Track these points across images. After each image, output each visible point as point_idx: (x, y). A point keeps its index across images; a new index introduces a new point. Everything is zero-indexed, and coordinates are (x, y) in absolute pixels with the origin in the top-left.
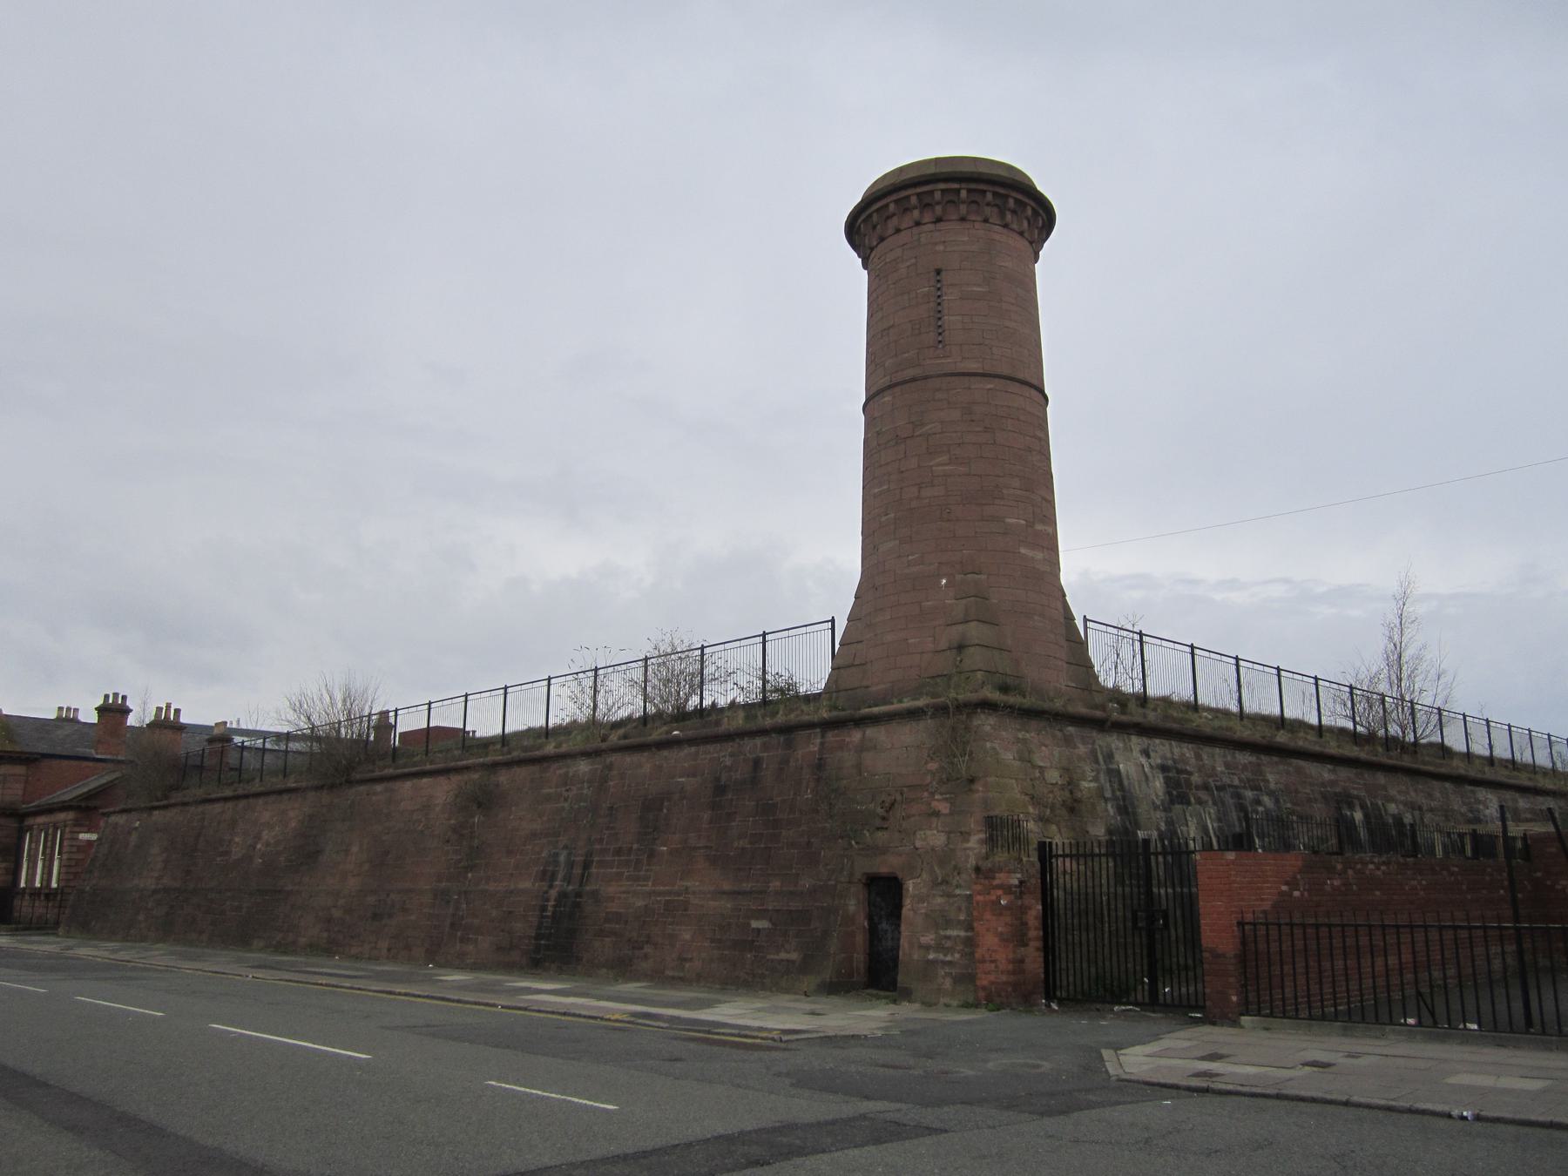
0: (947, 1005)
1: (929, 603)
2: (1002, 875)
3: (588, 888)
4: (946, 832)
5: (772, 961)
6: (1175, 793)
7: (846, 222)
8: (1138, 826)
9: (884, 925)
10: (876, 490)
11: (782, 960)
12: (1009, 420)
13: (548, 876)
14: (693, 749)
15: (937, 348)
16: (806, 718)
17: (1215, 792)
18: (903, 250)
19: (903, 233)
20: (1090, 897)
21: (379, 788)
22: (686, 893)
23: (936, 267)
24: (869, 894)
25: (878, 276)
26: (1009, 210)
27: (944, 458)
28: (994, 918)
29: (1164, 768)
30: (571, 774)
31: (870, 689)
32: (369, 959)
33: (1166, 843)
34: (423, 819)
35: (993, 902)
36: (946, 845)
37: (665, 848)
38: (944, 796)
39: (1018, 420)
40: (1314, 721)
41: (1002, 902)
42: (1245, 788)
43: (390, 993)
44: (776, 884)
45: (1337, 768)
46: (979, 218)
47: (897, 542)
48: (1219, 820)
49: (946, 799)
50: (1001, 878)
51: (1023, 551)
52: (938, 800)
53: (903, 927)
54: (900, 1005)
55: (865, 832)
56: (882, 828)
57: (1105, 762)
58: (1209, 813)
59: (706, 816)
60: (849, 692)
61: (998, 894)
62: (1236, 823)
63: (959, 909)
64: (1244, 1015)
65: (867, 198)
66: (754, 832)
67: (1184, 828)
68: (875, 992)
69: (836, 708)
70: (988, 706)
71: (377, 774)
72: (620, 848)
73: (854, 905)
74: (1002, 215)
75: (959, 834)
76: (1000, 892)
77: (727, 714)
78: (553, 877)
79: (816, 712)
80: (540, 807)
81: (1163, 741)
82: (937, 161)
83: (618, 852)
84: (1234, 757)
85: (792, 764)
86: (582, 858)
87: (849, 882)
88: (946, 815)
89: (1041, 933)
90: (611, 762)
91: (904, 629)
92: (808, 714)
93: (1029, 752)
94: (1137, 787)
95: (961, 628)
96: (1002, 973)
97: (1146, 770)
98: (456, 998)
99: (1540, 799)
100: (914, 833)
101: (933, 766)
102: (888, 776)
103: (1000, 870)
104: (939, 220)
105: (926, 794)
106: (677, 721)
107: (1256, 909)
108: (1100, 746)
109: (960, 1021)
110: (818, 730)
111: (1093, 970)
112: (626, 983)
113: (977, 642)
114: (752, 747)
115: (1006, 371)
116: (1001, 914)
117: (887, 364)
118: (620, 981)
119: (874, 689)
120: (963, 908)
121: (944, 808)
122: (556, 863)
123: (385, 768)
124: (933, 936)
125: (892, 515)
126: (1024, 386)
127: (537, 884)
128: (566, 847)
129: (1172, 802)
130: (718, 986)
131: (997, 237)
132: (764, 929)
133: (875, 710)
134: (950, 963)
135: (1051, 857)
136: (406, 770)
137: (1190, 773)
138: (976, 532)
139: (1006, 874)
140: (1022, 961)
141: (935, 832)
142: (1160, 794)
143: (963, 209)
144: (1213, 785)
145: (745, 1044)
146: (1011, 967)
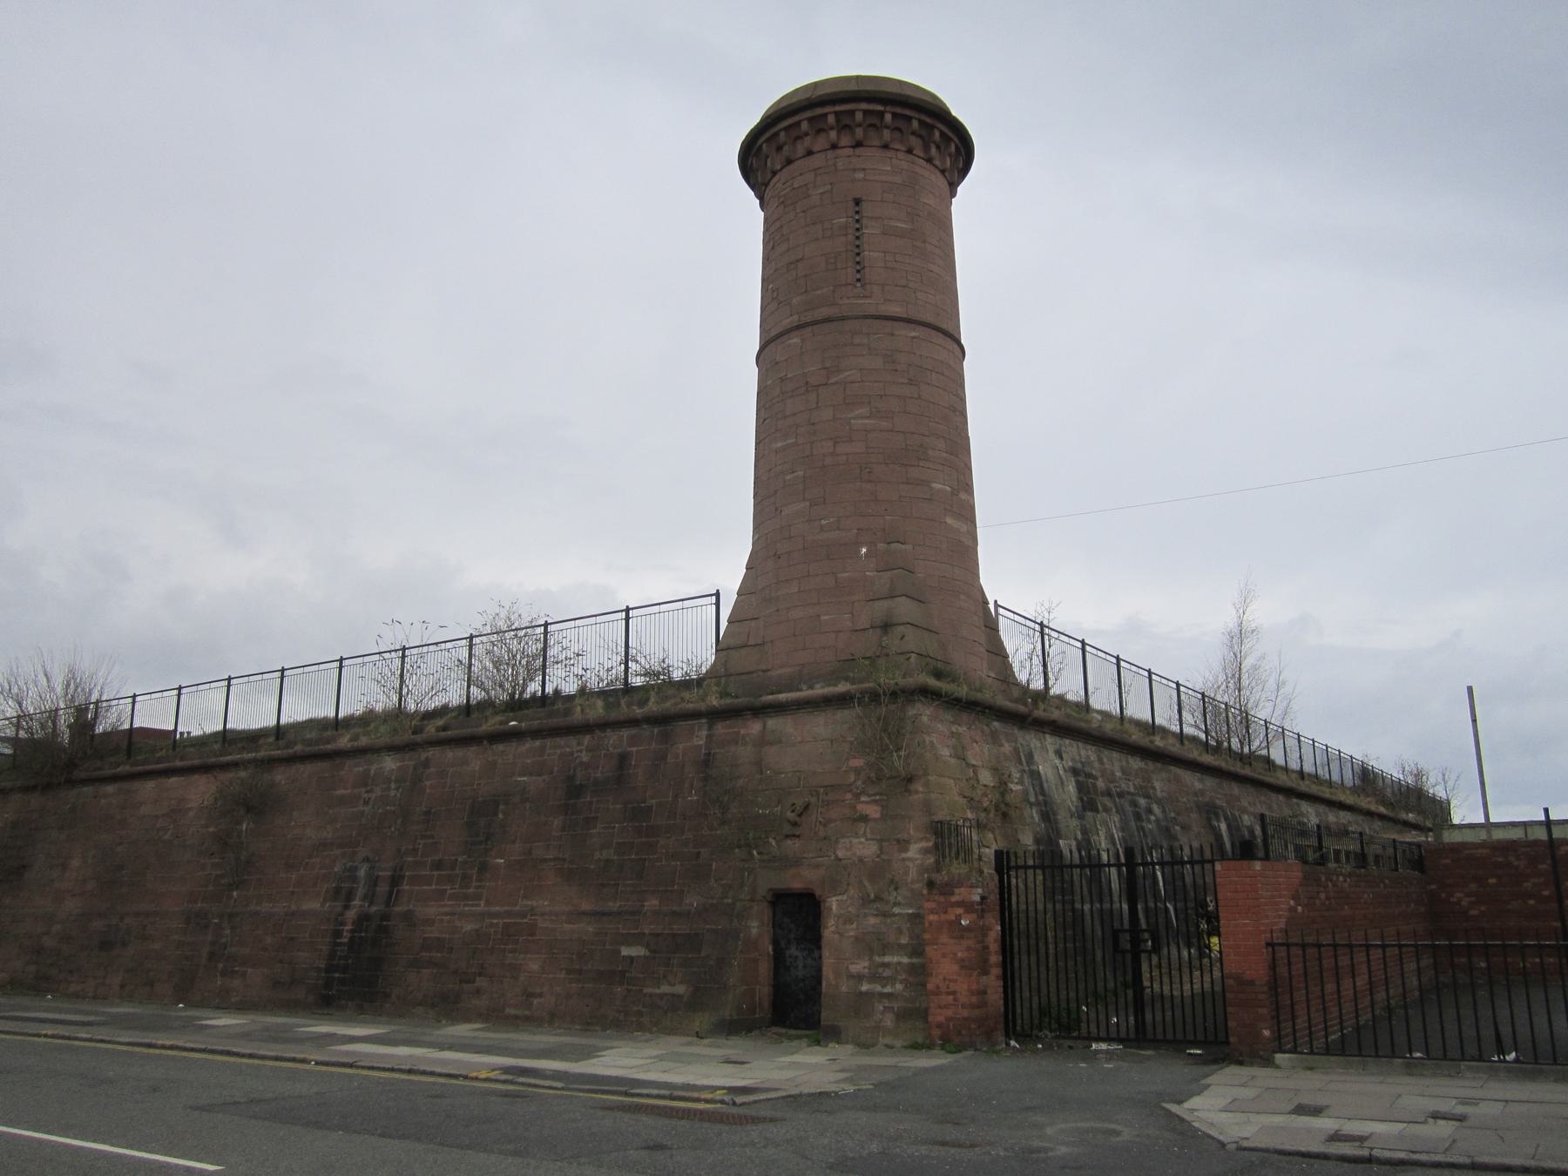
1: (847, 574)
3: (398, 909)
4: (877, 840)
6: (1085, 799)
7: (743, 142)
8: (1059, 835)
9: (793, 951)
10: (780, 444)
11: (666, 994)
13: (344, 895)
14: (538, 743)
15: (855, 287)
18: (816, 175)
20: (1032, 914)
21: (110, 789)
22: (532, 915)
25: (782, 202)
28: (952, 941)
29: (1075, 772)
31: (769, 673)
32: (95, 998)
33: (1083, 853)
35: (951, 923)
36: (878, 857)
37: (502, 861)
38: (873, 798)
39: (943, 374)
40: (1176, 729)
41: (963, 922)
43: (150, 1046)
44: (652, 903)
45: (1204, 777)
47: (808, 504)
48: (1123, 830)
49: (875, 802)
50: (960, 894)
51: (949, 520)
52: (863, 802)
53: (826, 953)
54: (827, 1046)
55: (771, 840)
56: (794, 836)
57: (1027, 762)
58: (1114, 822)
59: (556, 822)
60: (743, 677)
61: (958, 913)
62: (1136, 833)
64: (1276, 1052)
66: (620, 841)
67: (1095, 837)
69: (728, 695)
70: (926, 693)
71: (108, 772)
72: (440, 860)
73: (757, 927)
74: (926, 148)
75: (895, 843)
76: (960, 911)
77: (577, 701)
78: (350, 896)
80: (331, 811)
81: (1072, 742)
83: (438, 865)
84: (1127, 762)
85: (670, 759)
86: (389, 873)
88: (875, 820)
89: (1001, 958)
90: (427, 758)
91: (815, 604)
92: (691, 702)
93: (963, 748)
94: (1055, 790)
95: (885, 604)
97: (1061, 772)
98: (248, 1051)
100: (837, 842)
101: (858, 763)
103: (960, 884)
104: (859, 144)
105: (849, 796)
106: (512, 710)
107: (1274, 928)
108: (1021, 745)
109: (878, 1067)
110: (704, 721)
111: (1035, 999)
114: (615, 740)
115: (929, 318)
116: (962, 937)
118: (444, 1022)
119: (774, 673)
121: (873, 811)
122: (354, 879)
124: (866, 964)
125: (801, 473)
126: (947, 338)
127: (328, 905)
128: (367, 860)
129: (1084, 809)
131: (918, 169)
132: (638, 957)
133: (782, 697)
134: (889, 996)
135: (1009, 868)
137: (1095, 778)
139: (968, 889)
141: (863, 840)
142: (1074, 799)
143: (887, 134)
144: (1114, 790)
145: (677, 1110)
146: (974, 999)
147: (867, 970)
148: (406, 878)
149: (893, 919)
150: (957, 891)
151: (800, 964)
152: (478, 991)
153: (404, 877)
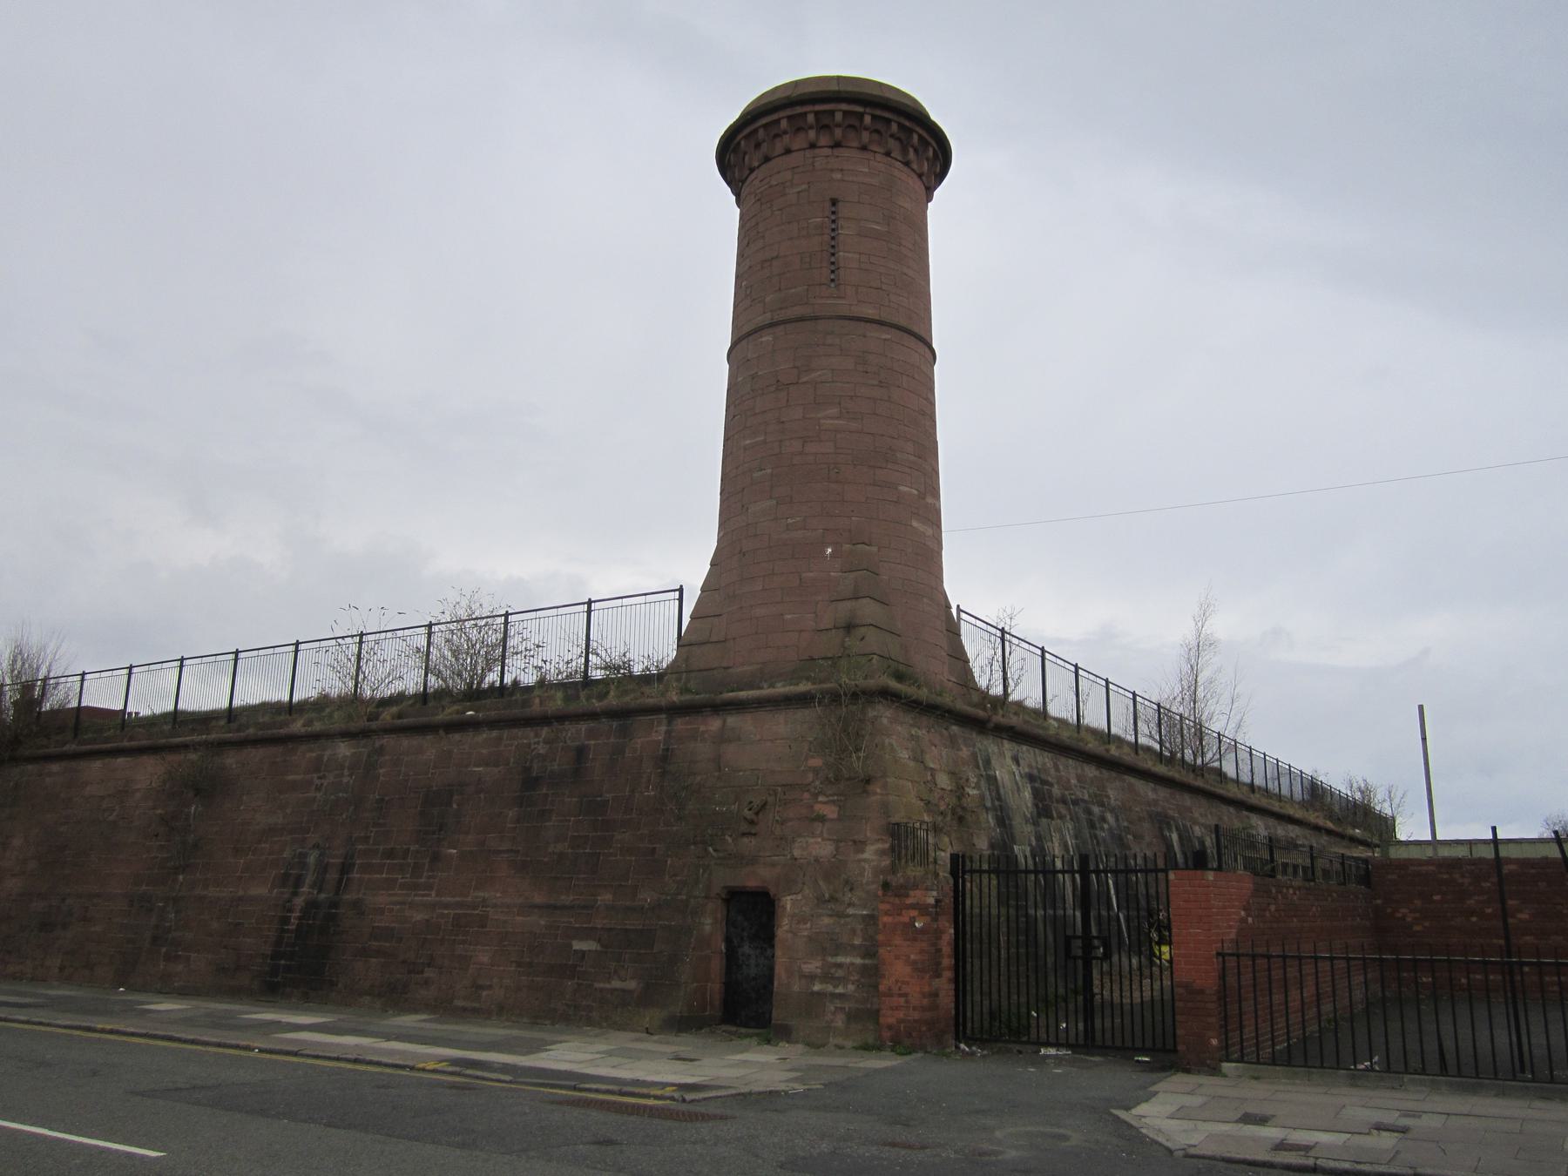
0: (841, 1047)
1: (811, 574)
2: (918, 893)
5: (601, 990)
6: (1040, 805)
9: (746, 949)
10: (748, 442)
11: (616, 990)
12: (904, 377)
14: (495, 733)
16: (651, 701)
17: (1071, 807)
19: (794, 154)
20: (985, 919)
21: (55, 767)
23: (833, 197)
24: (728, 911)
26: (912, 146)
27: (834, 411)
28: (908, 943)
29: (1031, 778)
30: (325, 758)
32: (32, 979)
34: (117, 807)
36: (834, 856)
37: (455, 851)
38: (831, 798)
40: (1131, 738)
41: (917, 924)
42: (1094, 804)
43: (89, 1029)
45: (1158, 787)
46: (882, 151)
47: (775, 502)
48: (1076, 838)
49: (833, 802)
50: (915, 896)
51: (915, 524)
53: (778, 953)
54: (776, 1046)
55: (727, 837)
60: (705, 673)
62: (1089, 841)
63: (854, 931)
65: (753, 110)
66: (576, 834)
67: (1050, 844)
68: (734, 1029)
69: (687, 691)
71: (52, 750)
73: (710, 924)
74: (904, 151)
75: (850, 843)
76: (914, 913)
77: (537, 692)
78: (299, 881)
79: (663, 694)
82: (839, 79)
83: (390, 854)
84: (1083, 770)
86: (340, 861)
87: (706, 897)
88: (832, 820)
90: (382, 746)
92: (652, 696)
95: (849, 604)
96: (915, 1008)
99: (1290, 827)
102: (756, 772)
103: (915, 887)
104: (837, 145)
105: (806, 795)
108: (980, 750)
110: (664, 716)
111: (986, 1003)
112: (399, 1015)
113: (869, 621)
114: (575, 733)
115: (903, 322)
116: (915, 940)
117: (768, 299)
120: (859, 932)
121: (831, 812)
122: (303, 865)
123: (65, 744)
124: (819, 964)
125: (769, 471)
128: (316, 846)
129: (1039, 815)
130: (525, 1020)
131: (896, 173)
133: (743, 694)
134: (841, 996)
136: (97, 747)
137: (1051, 785)
138: (867, 498)
140: (937, 995)
141: (820, 840)
142: (1029, 805)
143: (866, 136)
146: (925, 1002)
147: (819, 971)
148: (357, 866)
149: (847, 919)
150: (912, 893)
151: (753, 962)
152: (427, 982)
153: (354, 865)
